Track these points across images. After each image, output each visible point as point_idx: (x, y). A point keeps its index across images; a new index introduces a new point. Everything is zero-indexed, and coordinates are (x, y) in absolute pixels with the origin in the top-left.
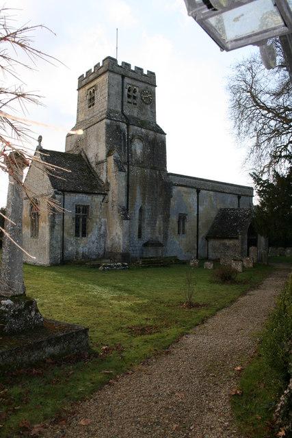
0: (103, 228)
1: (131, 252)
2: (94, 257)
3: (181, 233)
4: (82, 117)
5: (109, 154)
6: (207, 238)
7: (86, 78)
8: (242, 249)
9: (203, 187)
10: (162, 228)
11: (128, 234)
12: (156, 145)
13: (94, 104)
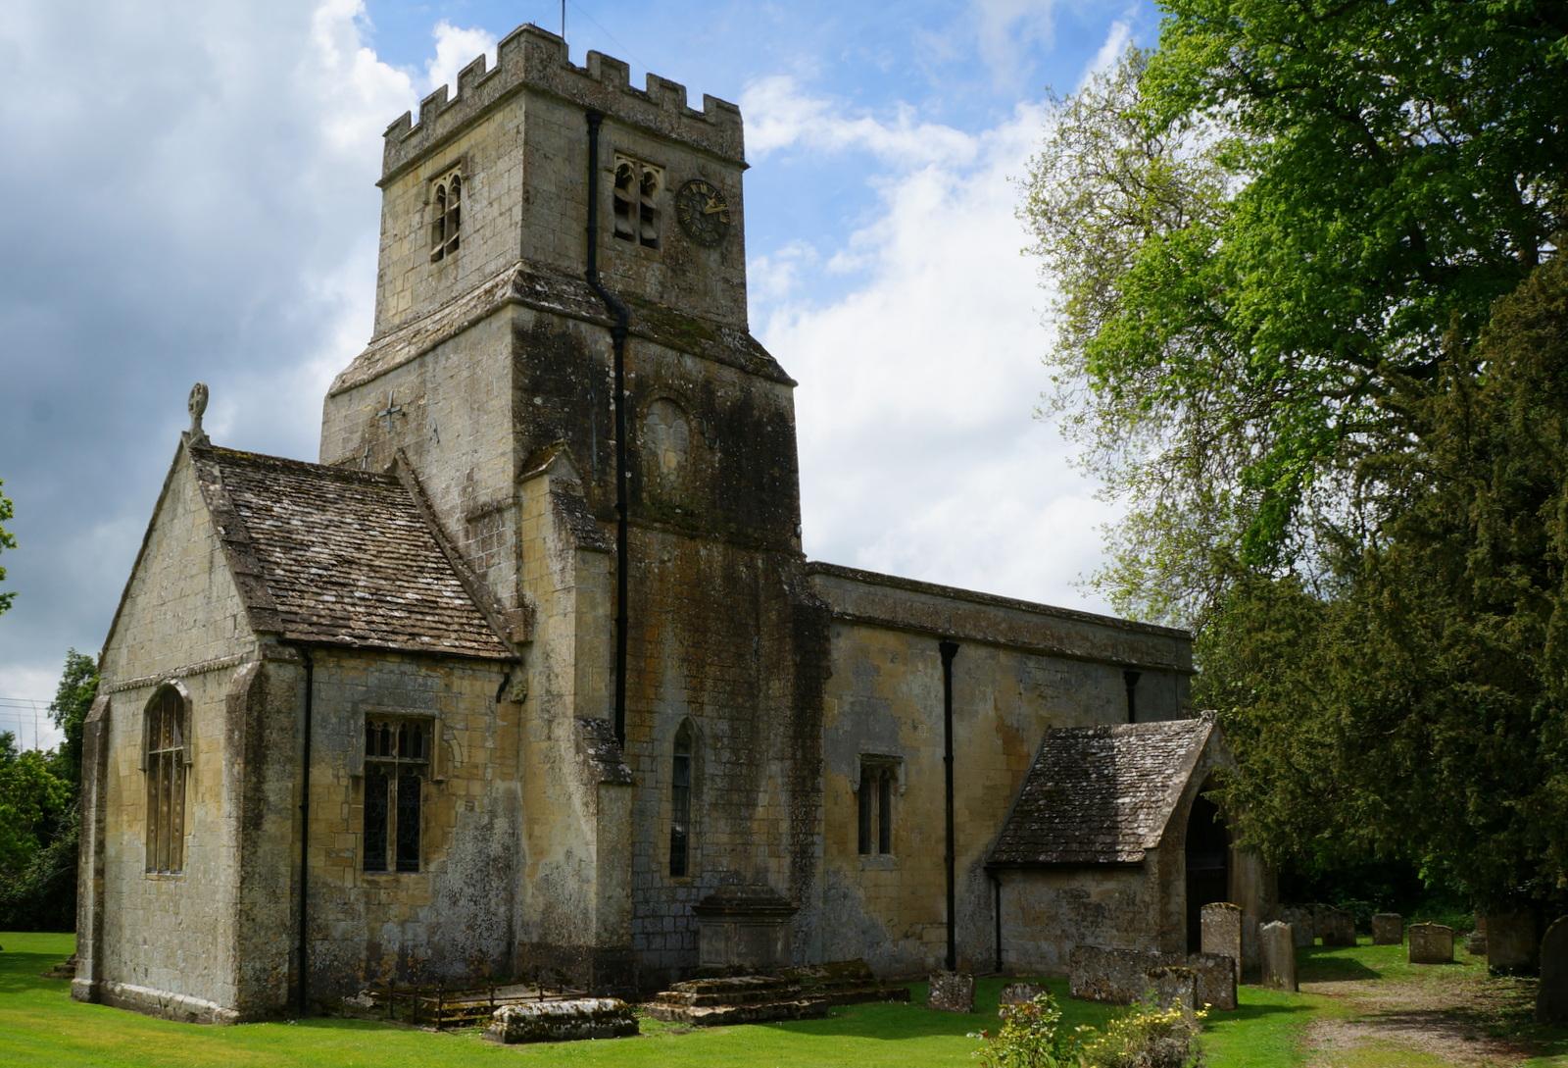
0: (501, 824)
1: (640, 942)
2: (459, 969)
3: (875, 845)
4: (401, 305)
5: (527, 468)
6: (996, 871)
7: (420, 128)
8: (1165, 914)
9: (969, 630)
10: (785, 826)
11: (626, 855)
12: (753, 438)
13: (455, 245)
